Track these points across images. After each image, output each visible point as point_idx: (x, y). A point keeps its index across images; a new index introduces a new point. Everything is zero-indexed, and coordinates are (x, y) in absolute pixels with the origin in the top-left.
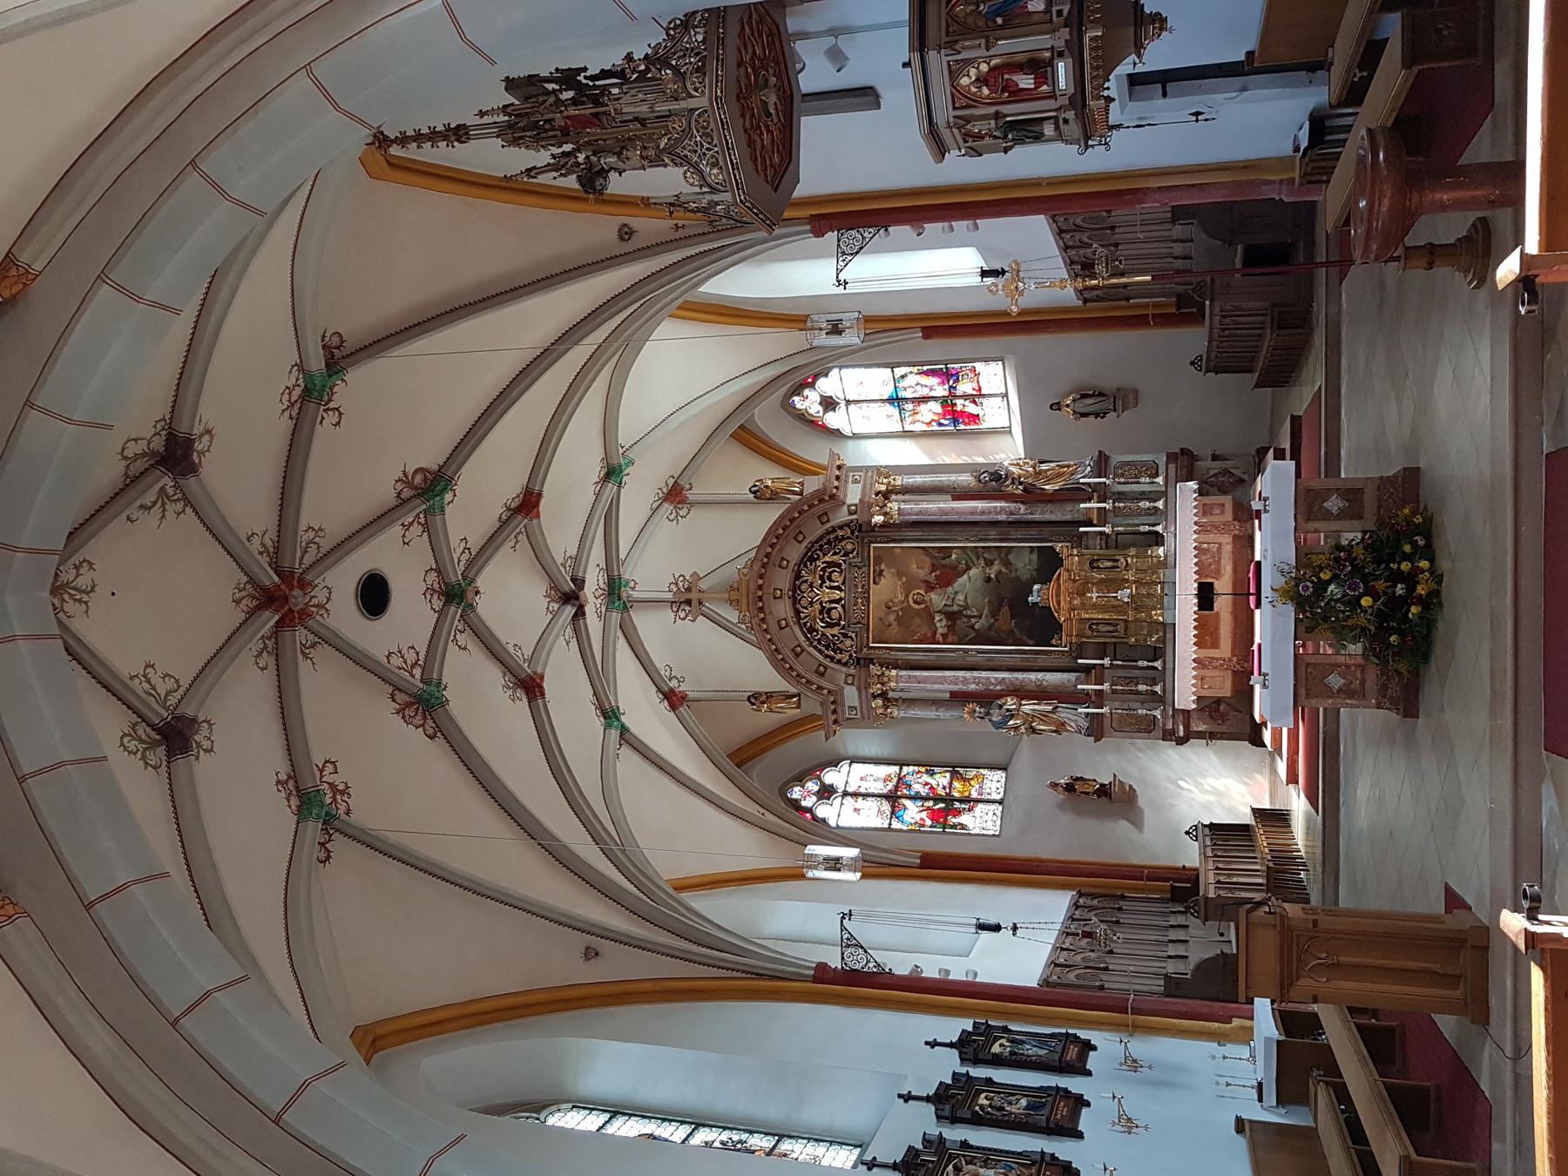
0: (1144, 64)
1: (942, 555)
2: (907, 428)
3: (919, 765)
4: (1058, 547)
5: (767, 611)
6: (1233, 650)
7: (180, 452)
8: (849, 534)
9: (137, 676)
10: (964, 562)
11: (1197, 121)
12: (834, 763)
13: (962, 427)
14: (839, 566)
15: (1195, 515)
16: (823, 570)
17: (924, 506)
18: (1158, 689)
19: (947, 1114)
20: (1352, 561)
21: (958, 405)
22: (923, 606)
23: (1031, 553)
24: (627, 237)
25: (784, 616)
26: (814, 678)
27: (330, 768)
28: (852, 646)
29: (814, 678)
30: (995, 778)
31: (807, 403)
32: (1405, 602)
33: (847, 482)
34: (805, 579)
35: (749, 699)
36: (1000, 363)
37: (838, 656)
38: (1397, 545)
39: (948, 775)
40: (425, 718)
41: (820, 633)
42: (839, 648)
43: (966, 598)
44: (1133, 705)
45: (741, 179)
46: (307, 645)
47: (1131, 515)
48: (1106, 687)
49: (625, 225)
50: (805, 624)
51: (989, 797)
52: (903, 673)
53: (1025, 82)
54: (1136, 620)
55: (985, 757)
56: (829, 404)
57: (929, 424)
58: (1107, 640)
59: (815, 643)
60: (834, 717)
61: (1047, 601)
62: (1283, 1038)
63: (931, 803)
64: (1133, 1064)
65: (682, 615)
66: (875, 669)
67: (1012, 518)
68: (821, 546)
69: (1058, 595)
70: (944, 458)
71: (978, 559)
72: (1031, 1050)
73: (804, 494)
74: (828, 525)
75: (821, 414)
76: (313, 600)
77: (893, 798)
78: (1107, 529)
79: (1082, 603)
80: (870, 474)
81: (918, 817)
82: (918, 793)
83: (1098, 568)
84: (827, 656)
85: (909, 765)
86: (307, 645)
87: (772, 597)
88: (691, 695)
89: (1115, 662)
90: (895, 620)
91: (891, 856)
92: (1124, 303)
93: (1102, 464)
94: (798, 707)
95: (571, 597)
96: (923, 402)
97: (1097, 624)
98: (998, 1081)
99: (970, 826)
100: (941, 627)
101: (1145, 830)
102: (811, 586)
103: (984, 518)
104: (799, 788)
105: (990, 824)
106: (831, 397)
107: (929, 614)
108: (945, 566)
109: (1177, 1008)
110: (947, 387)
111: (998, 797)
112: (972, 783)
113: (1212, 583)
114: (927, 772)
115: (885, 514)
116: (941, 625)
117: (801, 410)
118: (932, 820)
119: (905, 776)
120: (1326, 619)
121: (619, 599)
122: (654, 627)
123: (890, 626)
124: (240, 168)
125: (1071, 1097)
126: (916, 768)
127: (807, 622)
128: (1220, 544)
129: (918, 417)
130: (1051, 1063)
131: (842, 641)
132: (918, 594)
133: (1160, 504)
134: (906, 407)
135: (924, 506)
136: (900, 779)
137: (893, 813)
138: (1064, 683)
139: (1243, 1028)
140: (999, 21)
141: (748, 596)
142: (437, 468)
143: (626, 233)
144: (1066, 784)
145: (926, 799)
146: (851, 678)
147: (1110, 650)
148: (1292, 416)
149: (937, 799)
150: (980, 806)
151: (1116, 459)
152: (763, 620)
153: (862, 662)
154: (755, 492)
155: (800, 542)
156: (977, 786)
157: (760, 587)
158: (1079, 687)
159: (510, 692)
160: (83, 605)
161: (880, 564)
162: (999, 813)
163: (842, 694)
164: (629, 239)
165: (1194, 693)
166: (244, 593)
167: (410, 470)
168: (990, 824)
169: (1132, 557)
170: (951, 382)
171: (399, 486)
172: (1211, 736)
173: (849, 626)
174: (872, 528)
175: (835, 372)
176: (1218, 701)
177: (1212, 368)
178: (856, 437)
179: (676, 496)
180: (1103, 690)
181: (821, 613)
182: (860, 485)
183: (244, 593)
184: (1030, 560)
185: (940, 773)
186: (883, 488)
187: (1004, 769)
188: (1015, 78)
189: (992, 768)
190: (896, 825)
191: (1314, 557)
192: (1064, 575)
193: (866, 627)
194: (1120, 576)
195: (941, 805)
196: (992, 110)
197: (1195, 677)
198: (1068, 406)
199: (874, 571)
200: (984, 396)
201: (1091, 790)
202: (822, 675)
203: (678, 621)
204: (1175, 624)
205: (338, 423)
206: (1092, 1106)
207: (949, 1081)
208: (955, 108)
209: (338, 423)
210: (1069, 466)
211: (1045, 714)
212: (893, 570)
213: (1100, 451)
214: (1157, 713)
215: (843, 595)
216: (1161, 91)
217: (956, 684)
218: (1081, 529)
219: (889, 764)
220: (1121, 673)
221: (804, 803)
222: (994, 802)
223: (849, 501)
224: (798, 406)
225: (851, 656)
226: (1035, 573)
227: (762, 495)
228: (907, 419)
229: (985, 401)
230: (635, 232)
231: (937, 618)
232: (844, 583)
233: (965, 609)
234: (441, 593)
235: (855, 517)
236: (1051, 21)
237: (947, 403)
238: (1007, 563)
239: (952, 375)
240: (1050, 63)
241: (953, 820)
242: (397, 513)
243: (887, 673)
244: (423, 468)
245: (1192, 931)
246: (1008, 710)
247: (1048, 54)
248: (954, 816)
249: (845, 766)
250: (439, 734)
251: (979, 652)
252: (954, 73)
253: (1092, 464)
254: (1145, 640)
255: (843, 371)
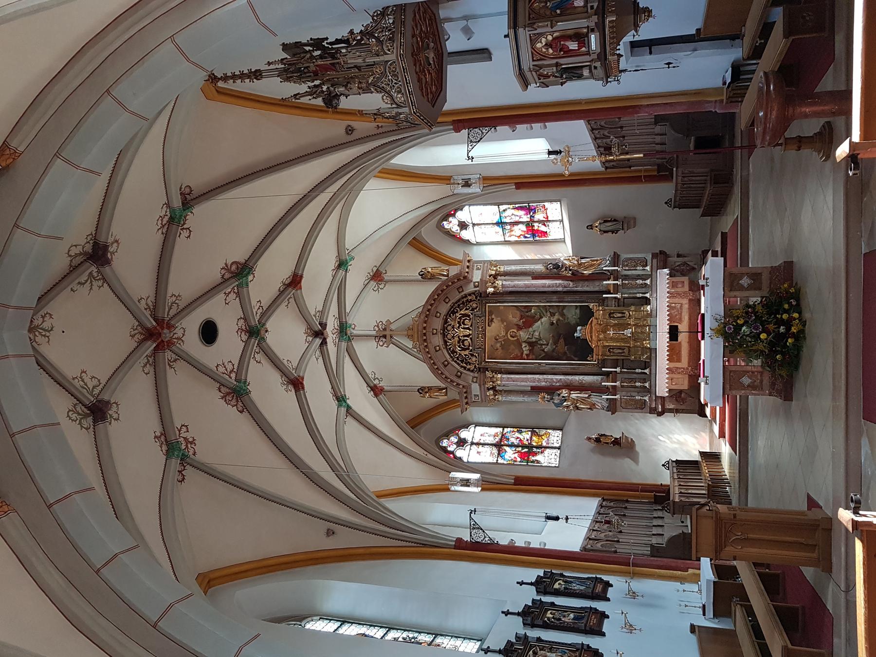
0: (639, 36)
1: (526, 310)
2: (507, 239)
3: (513, 428)
4: (591, 305)
5: (428, 341)
6: (689, 363)
7: (100, 252)
8: (474, 299)
9: (76, 378)
10: (538, 314)
11: (669, 67)
12: (466, 426)
13: (537, 238)
14: (469, 316)
15: (668, 288)
16: (460, 318)
17: (516, 282)
18: (647, 385)
19: (529, 623)
20: (755, 313)
21: (535, 226)
22: (516, 338)
23: (576, 309)
24: (350, 132)
25: (438, 344)
26: (455, 379)
27: (184, 429)
28: (476, 361)
29: (455, 379)
30: (556, 435)
31: (451, 225)
32: (785, 336)
33: (473, 269)
34: (450, 323)
35: (418, 391)
36: (559, 203)
37: (468, 367)
38: (781, 304)
39: (530, 433)
40: (237, 401)
41: (458, 354)
42: (468, 362)
43: (540, 334)
44: (633, 394)
45: (414, 100)
46: (172, 360)
47: (632, 288)
48: (618, 384)
49: (349, 126)
50: (450, 348)
51: (552, 445)
52: (504, 376)
53: (573, 46)
54: (635, 346)
55: (550, 423)
56: (463, 225)
57: (519, 237)
58: (619, 358)
59: (455, 359)
60: (466, 401)
61: (585, 336)
62: (717, 580)
63: (520, 449)
64: (633, 595)
65: (381, 343)
66: (489, 374)
67: (565, 289)
68: (459, 305)
69: (591, 333)
70: (528, 256)
71: (546, 312)
72: (576, 587)
73: (449, 276)
74: (463, 294)
75: (459, 231)
76: (175, 335)
77: (499, 446)
78: (618, 296)
79: (605, 337)
80: (486, 265)
81: (513, 457)
82: (513, 443)
83: (614, 317)
84: (462, 367)
85: (508, 427)
86: (172, 360)
87: (431, 333)
88: (386, 388)
89: (623, 370)
90: (500, 346)
91: (498, 478)
92: (628, 169)
93: (616, 259)
94: (446, 395)
95: (319, 333)
96: (516, 224)
97: (613, 349)
98: (557, 604)
99: (542, 461)
100: (526, 350)
101: (640, 464)
102: (453, 327)
103: (550, 289)
104: (446, 440)
105: (553, 461)
106: (464, 222)
107: (519, 343)
108: (528, 316)
109: (657, 563)
110: (529, 216)
111: (558, 445)
112: (543, 437)
113: (677, 326)
114: (518, 431)
115: (495, 287)
116: (526, 349)
117: (448, 229)
118: (521, 458)
119: (505, 433)
120: (741, 346)
121: (346, 335)
122: (365, 350)
123: (497, 349)
124: (134, 94)
125: (598, 613)
126: (512, 429)
127: (451, 347)
128: (682, 304)
129: (513, 233)
130: (587, 594)
131: (470, 358)
132: (513, 332)
133: (648, 282)
134: (506, 227)
135: (516, 282)
136: (503, 435)
137: (499, 454)
138: (594, 382)
139: (694, 574)
140: (558, 11)
141: (418, 333)
142: (244, 261)
143: (350, 130)
144: (595, 438)
145: (517, 446)
146: (475, 379)
147: (620, 363)
148: (722, 232)
149: (524, 447)
150: (548, 450)
151: (624, 256)
152: (426, 346)
153: (482, 370)
154: (422, 275)
155: (447, 303)
156: (546, 439)
157: (425, 328)
158: (603, 384)
159: (285, 387)
160: (47, 338)
161: (492, 315)
162: (558, 454)
163: (470, 388)
164: (352, 133)
165: (667, 387)
166: (136, 332)
167: (229, 262)
168: (553, 461)
169: (633, 311)
170: (531, 214)
171: (223, 272)
172: (677, 411)
173: (474, 350)
174: (487, 295)
175: (466, 208)
176: (681, 391)
177: (677, 206)
178: (478, 244)
179: (378, 277)
180: (616, 386)
181: (459, 342)
182: (480, 271)
183: (136, 332)
184: (575, 313)
185: (525, 432)
186: (493, 273)
187: (561, 430)
188: (567, 43)
189: (554, 429)
190: (500, 461)
191: (734, 311)
192: (595, 321)
193: (484, 350)
194: (626, 322)
195: (526, 450)
196: (554, 61)
197: (667, 378)
198: (596, 227)
199: (488, 319)
200: (549, 221)
201: (609, 441)
202: (459, 377)
203: (379, 347)
204: (656, 349)
205: (189, 236)
206: (610, 618)
207: (530, 604)
208: (533, 60)
209: (189, 236)
210: (597, 260)
211: (584, 399)
212: (499, 319)
213: (614, 252)
214: (647, 398)
215: (471, 332)
216: (648, 51)
217: (534, 382)
218: (604, 296)
219: (496, 427)
220: (626, 376)
221: (449, 449)
222: (555, 448)
223: (474, 280)
224: (446, 227)
225: (475, 366)
226: (578, 320)
227: (425, 276)
228: (506, 234)
229: (550, 224)
230: (355, 129)
231: (524, 345)
232: (471, 326)
233: (539, 340)
234: (246, 331)
235: (477, 289)
236: (587, 12)
237: (529, 225)
238: (563, 315)
239: (532, 210)
240: (587, 35)
241: (532, 458)
242: (222, 287)
243: (495, 376)
244: (236, 262)
245: (666, 520)
246: (563, 397)
247: (585, 30)
248: (533, 456)
249: (472, 428)
250: (245, 410)
251: (547, 364)
252: (533, 41)
253: (610, 259)
254: (640, 358)
255: (471, 207)
